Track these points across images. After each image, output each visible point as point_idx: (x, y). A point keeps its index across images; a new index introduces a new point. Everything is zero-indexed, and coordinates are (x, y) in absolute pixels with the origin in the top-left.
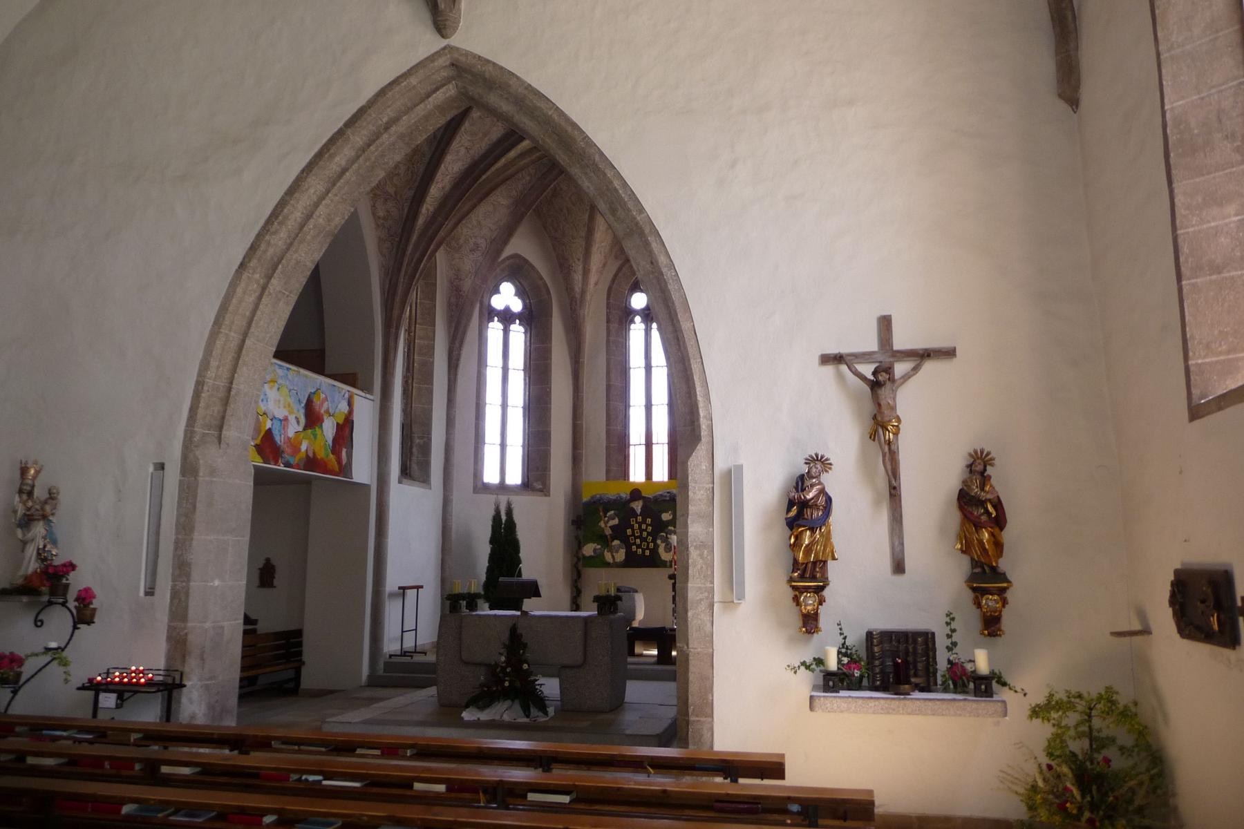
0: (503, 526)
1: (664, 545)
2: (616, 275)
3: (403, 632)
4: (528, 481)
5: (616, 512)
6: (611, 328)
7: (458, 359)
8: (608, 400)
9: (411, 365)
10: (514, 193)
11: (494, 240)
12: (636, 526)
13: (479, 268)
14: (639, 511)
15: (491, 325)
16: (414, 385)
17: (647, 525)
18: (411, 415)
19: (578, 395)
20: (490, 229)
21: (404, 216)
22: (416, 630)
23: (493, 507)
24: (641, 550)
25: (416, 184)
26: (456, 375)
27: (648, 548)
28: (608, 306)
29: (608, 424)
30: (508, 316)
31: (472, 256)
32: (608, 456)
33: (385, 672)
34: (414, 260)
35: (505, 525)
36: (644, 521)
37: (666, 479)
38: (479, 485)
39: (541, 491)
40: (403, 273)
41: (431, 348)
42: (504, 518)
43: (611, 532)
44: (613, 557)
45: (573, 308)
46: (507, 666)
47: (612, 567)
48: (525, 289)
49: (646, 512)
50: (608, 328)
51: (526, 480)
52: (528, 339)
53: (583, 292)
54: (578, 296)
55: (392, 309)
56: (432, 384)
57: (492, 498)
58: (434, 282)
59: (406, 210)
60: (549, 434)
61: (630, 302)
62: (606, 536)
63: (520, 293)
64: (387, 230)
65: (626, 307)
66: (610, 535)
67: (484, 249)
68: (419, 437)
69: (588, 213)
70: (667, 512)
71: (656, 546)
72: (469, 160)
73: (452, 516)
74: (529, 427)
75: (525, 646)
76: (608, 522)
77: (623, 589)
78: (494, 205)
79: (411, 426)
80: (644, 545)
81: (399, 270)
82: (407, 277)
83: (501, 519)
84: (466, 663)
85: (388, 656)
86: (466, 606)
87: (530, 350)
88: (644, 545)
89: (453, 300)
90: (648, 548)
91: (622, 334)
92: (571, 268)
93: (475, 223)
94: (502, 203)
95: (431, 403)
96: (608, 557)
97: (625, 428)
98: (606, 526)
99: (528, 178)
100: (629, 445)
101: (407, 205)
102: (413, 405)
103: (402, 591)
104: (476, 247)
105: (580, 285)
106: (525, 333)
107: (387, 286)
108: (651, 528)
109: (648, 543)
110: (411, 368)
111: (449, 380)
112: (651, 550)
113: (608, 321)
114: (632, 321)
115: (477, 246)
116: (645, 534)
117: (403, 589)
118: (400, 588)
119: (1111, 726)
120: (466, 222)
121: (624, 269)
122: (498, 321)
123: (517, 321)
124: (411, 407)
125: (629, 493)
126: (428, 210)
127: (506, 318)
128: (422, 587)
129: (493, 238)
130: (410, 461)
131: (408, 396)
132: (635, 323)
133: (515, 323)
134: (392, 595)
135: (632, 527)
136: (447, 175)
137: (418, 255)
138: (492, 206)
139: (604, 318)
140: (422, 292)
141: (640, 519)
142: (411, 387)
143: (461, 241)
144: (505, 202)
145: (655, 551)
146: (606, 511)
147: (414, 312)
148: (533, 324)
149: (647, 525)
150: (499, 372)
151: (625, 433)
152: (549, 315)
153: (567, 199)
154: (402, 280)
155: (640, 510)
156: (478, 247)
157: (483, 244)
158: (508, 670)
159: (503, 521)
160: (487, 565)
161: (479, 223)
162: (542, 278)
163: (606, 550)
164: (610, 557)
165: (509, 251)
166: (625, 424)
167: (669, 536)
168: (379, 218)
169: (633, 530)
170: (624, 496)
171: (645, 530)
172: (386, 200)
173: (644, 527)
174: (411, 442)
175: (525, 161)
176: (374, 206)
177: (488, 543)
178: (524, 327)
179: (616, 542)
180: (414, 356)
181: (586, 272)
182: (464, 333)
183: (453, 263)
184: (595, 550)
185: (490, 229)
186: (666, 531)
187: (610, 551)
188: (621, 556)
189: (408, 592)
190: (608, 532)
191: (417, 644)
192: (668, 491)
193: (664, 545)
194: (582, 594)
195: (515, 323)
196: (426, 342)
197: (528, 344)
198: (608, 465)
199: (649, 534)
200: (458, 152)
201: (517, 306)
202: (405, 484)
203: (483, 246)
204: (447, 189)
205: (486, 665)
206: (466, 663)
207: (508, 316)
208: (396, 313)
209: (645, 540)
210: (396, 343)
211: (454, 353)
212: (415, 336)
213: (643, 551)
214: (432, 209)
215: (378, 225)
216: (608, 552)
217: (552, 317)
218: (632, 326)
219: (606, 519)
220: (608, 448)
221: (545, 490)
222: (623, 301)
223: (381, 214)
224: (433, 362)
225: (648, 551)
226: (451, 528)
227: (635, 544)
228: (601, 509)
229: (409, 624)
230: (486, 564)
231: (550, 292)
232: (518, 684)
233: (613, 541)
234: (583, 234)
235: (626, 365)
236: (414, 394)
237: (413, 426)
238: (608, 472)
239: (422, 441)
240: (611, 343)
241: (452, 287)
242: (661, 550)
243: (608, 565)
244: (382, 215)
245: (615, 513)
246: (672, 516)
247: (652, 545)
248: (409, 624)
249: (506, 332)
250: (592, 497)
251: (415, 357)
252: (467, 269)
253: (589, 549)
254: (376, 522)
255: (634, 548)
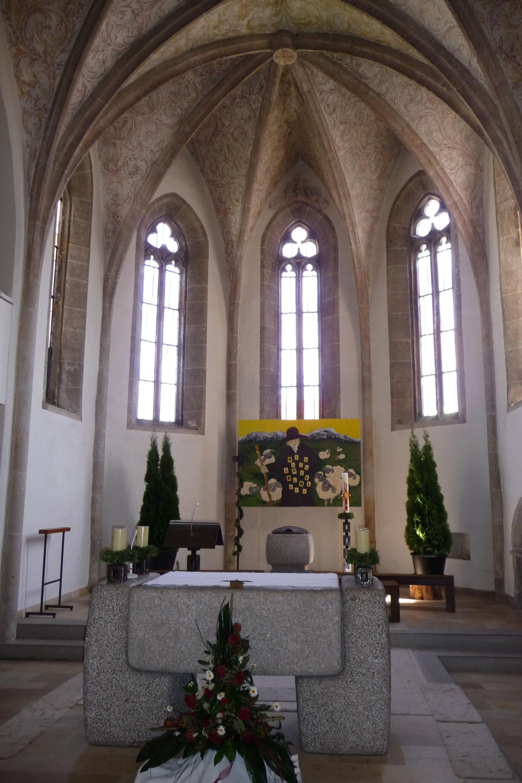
0: (159, 462)
1: (321, 483)
2: (270, 223)
3: (43, 584)
4: (182, 419)
5: (273, 450)
6: (265, 274)
7: (114, 288)
8: (262, 341)
9: (62, 286)
10: (179, 111)
11: (155, 162)
12: (293, 465)
13: (138, 192)
14: (296, 450)
15: (147, 262)
16: (65, 307)
17: (305, 464)
18: (61, 338)
19: (232, 336)
20: (151, 150)
21: (56, 87)
22: (60, 580)
23: (150, 442)
24: (298, 489)
25: (71, 45)
26: (111, 303)
27: (305, 487)
28: (263, 252)
29: (262, 365)
30: (165, 256)
31: (131, 180)
32: (262, 395)
33: (18, 637)
34: (67, 145)
35: (161, 461)
36: (301, 460)
37: (317, 417)
38: (134, 421)
39: (196, 429)
40: (52, 156)
41: (85, 272)
42: (161, 453)
43: (267, 471)
44: (270, 496)
45: (229, 252)
46: (217, 690)
47: (268, 506)
48: (181, 231)
49: (303, 450)
50: (262, 274)
51: (180, 418)
52: (184, 279)
53: (241, 232)
54: (234, 239)
55: (38, 198)
56: (85, 308)
57: (148, 434)
58: (90, 201)
59: (58, 79)
60: (204, 371)
61: (303, 227)
62: (263, 474)
63: (176, 234)
64: (33, 102)
65: (278, 255)
66: (267, 474)
67: (145, 171)
68: (69, 364)
69: (251, 148)
70: (324, 450)
71: (314, 485)
72: (135, 32)
73: (104, 451)
74: (183, 365)
75: (245, 645)
76: (264, 460)
77: (294, 531)
78: (156, 124)
79: (60, 351)
80: (301, 484)
81: (48, 152)
82: (57, 164)
83: (157, 455)
84: (138, 671)
85: (24, 615)
86: (133, 569)
87: (186, 291)
88: (301, 484)
89: (110, 227)
90: (305, 487)
91: (275, 280)
92: (228, 211)
93: (135, 143)
94: (165, 122)
95: (84, 328)
96: (264, 495)
97: (278, 370)
98: (262, 465)
99: (194, 95)
100: (281, 387)
101: (60, 72)
102: (63, 328)
103: (44, 535)
104: (136, 170)
105: (238, 226)
106: (181, 274)
107: (33, 172)
108: (308, 466)
109: (306, 482)
110: (62, 289)
111: (104, 308)
112: (308, 489)
113: (262, 266)
114: (284, 270)
115: (136, 170)
116: (302, 473)
117: (45, 533)
118: (41, 532)
119: (294, 545)
120: (126, 143)
121: (278, 217)
122: (154, 259)
123: (173, 262)
124: (61, 330)
125: (285, 431)
126: (84, 85)
127: (162, 256)
128: (68, 529)
129: (154, 160)
130: (59, 388)
131: (57, 318)
132: (286, 271)
133: (171, 264)
134: (31, 540)
135: (289, 466)
136: (109, 45)
137: (71, 139)
138: (154, 125)
139: (259, 264)
140: (77, 210)
141: (297, 457)
142: (61, 309)
143: (120, 164)
144: (168, 121)
145: (312, 490)
146: (262, 449)
147: (66, 229)
148: (189, 266)
149: (305, 464)
150: (154, 310)
151: (278, 376)
152: (205, 256)
153: (229, 136)
154: (51, 166)
155: (297, 449)
156: (137, 171)
157: (143, 167)
158: (219, 698)
159: (160, 458)
160: (142, 503)
161: (140, 144)
162: (198, 220)
163: (262, 489)
164: (266, 495)
165: (164, 188)
166: (278, 367)
167: (326, 475)
168: (24, 82)
169: (290, 469)
170: (280, 434)
171: (303, 469)
172: (33, 60)
173: (301, 465)
174: (61, 369)
175: (196, 58)
176: (17, 66)
177: (143, 479)
178: (180, 268)
179: (273, 481)
180: (65, 276)
181: (245, 211)
182: (121, 260)
183: (111, 187)
184: (251, 489)
185: (151, 150)
186: (324, 469)
187: (266, 489)
188: (277, 494)
189: (53, 536)
190: (264, 470)
191: (62, 594)
192: (325, 429)
193: (321, 483)
194: (243, 535)
195: (171, 264)
196: (79, 263)
197: (184, 284)
198: (262, 405)
199: (306, 473)
200: (123, 13)
201: (173, 247)
202: (50, 411)
203: (144, 168)
204: (109, 64)
205: (170, 674)
206: (138, 671)
207: (165, 256)
208: (43, 203)
209: (302, 478)
210: (43, 240)
211: (110, 281)
212: (67, 255)
213: (301, 489)
214: (90, 87)
215: (23, 93)
216: (264, 490)
217: (208, 258)
218: (284, 274)
219: (262, 457)
220: (261, 388)
221: (199, 429)
222: (275, 250)
223: (26, 78)
224: (87, 285)
225: (306, 490)
226: (103, 465)
227: (291, 482)
228: (257, 447)
229: (52, 574)
230: (141, 503)
231: (206, 235)
232: (239, 725)
233: (269, 479)
234: (244, 171)
235: (278, 310)
236: (64, 316)
237: (63, 351)
238: (262, 411)
239: (72, 369)
240: (265, 289)
241: (110, 213)
242: (319, 489)
243: (264, 504)
244: (28, 80)
245: (271, 452)
246: (329, 455)
247: (309, 484)
248: (52, 574)
249: (162, 271)
250: (248, 436)
251: (67, 277)
252: (126, 193)
253: (247, 488)
254: (11, 451)
255: (291, 486)
